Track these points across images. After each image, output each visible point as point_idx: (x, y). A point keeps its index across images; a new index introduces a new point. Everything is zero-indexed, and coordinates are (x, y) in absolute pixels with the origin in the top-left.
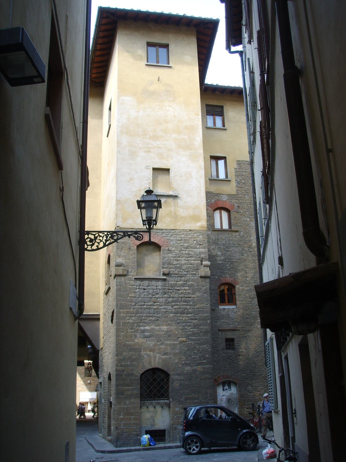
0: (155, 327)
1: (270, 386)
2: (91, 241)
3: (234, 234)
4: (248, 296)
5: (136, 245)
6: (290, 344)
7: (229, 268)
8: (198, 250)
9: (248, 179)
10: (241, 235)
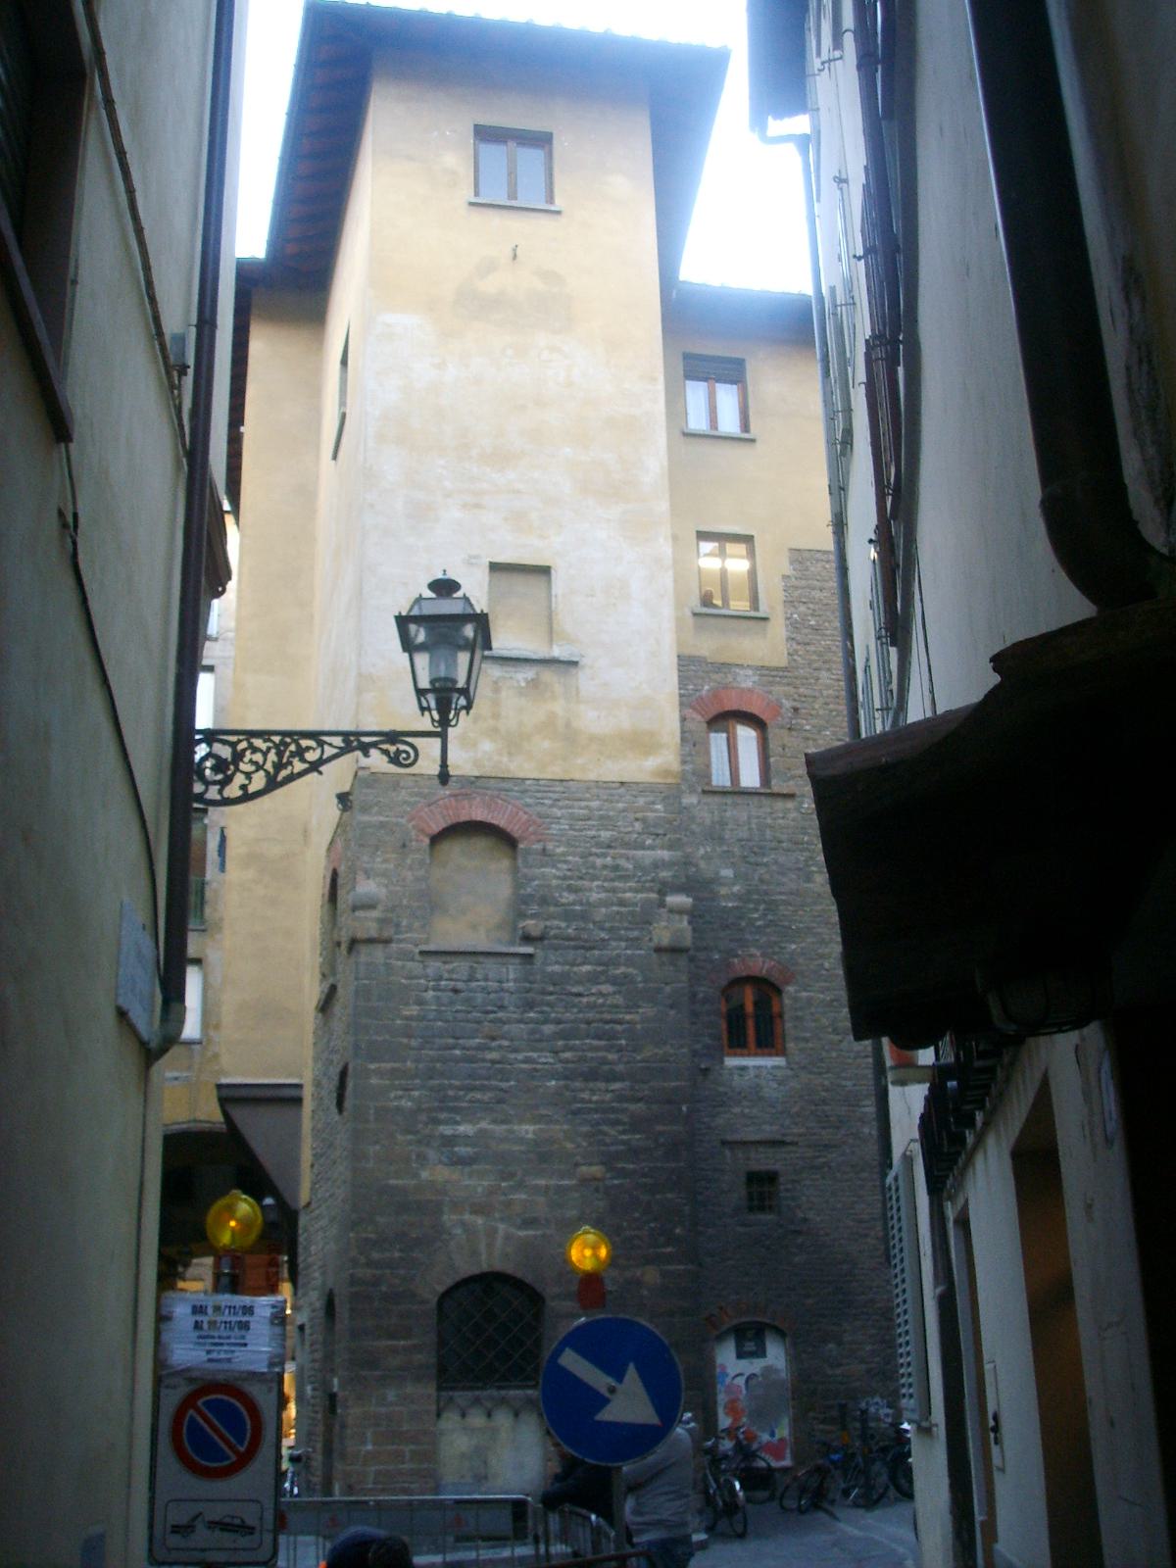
0: (491, 1126)
1: (903, 1325)
2: (221, 765)
3: (780, 804)
4: (827, 1024)
5: (427, 835)
6: (979, 1160)
7: (759, 923)
8: (647, 856)
9: (828, 613)
10: (803, 811)
